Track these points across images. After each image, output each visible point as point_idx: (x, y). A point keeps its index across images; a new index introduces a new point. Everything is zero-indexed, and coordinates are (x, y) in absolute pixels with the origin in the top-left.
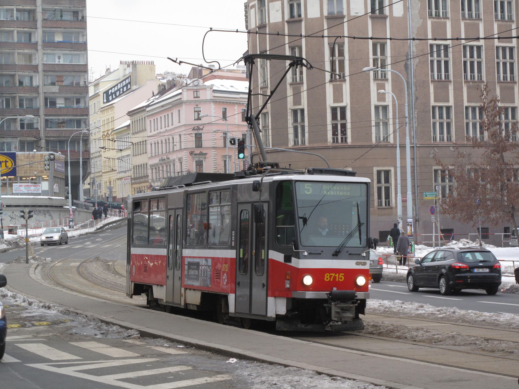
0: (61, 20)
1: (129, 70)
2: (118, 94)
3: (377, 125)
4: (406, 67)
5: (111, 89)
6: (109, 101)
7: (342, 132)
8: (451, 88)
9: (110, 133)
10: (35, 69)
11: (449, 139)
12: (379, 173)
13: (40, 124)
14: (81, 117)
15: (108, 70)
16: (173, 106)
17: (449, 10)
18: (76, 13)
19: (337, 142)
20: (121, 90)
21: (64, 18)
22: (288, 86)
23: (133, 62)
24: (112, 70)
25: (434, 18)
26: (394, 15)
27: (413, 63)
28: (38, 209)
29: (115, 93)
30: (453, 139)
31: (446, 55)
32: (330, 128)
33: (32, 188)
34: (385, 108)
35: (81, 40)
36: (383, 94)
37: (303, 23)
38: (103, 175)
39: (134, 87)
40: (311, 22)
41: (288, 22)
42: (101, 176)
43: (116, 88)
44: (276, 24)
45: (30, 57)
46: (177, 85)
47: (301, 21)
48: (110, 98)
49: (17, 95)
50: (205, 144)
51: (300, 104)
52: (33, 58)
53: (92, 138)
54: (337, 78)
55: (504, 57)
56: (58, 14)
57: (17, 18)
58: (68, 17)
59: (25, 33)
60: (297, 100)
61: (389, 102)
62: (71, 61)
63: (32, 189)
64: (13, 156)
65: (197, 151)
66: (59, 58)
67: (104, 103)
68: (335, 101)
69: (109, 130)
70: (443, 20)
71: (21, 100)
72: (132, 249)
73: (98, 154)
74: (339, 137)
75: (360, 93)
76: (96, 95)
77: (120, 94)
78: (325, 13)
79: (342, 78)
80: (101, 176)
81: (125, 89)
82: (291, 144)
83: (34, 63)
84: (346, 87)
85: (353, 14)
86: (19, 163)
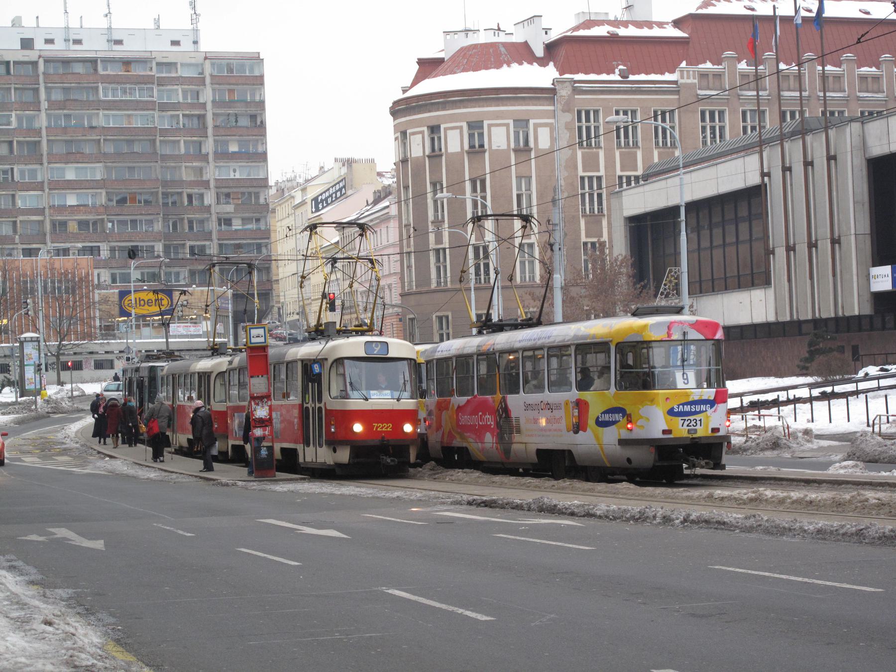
0: (236, 127)
1: (344, 170)
2: (329, 200)
5: (321, 194)
8: (605, 223)
10: (206, 184)
13: (213, 249)
16: (381, 222)
18: (253, 117)
19: (480, 282)
21: (239, 124)
22: (430, 224)
23: (348, 160)
24: (326, 169)
26: (540, 147)
28: (194, 353)
29: (326, 199)
33: (192, 329)
35: (260, 150)
37: (444, 158)
39: (349, 192)
41: (429, 157)
43: (327, 194)
44: (417, 158)
45: (201, 170)
47: (441, 155)
48: (320, 206)
49: (186, 216)
51: (442, 243)
52: (204, 172)
56: (233, 119)
57: (184, 125)
58: (244, 122)
59: (195, 142)
62: (249, 175)
63: (192, 330)
66: (235, 171)
71: (191, 222)
74: (482, 277)
76: (303, 203)
77: (332, 201)
81: (338, 194)
82: (434, 285)
83: (204, 178)
85: (494, 147)
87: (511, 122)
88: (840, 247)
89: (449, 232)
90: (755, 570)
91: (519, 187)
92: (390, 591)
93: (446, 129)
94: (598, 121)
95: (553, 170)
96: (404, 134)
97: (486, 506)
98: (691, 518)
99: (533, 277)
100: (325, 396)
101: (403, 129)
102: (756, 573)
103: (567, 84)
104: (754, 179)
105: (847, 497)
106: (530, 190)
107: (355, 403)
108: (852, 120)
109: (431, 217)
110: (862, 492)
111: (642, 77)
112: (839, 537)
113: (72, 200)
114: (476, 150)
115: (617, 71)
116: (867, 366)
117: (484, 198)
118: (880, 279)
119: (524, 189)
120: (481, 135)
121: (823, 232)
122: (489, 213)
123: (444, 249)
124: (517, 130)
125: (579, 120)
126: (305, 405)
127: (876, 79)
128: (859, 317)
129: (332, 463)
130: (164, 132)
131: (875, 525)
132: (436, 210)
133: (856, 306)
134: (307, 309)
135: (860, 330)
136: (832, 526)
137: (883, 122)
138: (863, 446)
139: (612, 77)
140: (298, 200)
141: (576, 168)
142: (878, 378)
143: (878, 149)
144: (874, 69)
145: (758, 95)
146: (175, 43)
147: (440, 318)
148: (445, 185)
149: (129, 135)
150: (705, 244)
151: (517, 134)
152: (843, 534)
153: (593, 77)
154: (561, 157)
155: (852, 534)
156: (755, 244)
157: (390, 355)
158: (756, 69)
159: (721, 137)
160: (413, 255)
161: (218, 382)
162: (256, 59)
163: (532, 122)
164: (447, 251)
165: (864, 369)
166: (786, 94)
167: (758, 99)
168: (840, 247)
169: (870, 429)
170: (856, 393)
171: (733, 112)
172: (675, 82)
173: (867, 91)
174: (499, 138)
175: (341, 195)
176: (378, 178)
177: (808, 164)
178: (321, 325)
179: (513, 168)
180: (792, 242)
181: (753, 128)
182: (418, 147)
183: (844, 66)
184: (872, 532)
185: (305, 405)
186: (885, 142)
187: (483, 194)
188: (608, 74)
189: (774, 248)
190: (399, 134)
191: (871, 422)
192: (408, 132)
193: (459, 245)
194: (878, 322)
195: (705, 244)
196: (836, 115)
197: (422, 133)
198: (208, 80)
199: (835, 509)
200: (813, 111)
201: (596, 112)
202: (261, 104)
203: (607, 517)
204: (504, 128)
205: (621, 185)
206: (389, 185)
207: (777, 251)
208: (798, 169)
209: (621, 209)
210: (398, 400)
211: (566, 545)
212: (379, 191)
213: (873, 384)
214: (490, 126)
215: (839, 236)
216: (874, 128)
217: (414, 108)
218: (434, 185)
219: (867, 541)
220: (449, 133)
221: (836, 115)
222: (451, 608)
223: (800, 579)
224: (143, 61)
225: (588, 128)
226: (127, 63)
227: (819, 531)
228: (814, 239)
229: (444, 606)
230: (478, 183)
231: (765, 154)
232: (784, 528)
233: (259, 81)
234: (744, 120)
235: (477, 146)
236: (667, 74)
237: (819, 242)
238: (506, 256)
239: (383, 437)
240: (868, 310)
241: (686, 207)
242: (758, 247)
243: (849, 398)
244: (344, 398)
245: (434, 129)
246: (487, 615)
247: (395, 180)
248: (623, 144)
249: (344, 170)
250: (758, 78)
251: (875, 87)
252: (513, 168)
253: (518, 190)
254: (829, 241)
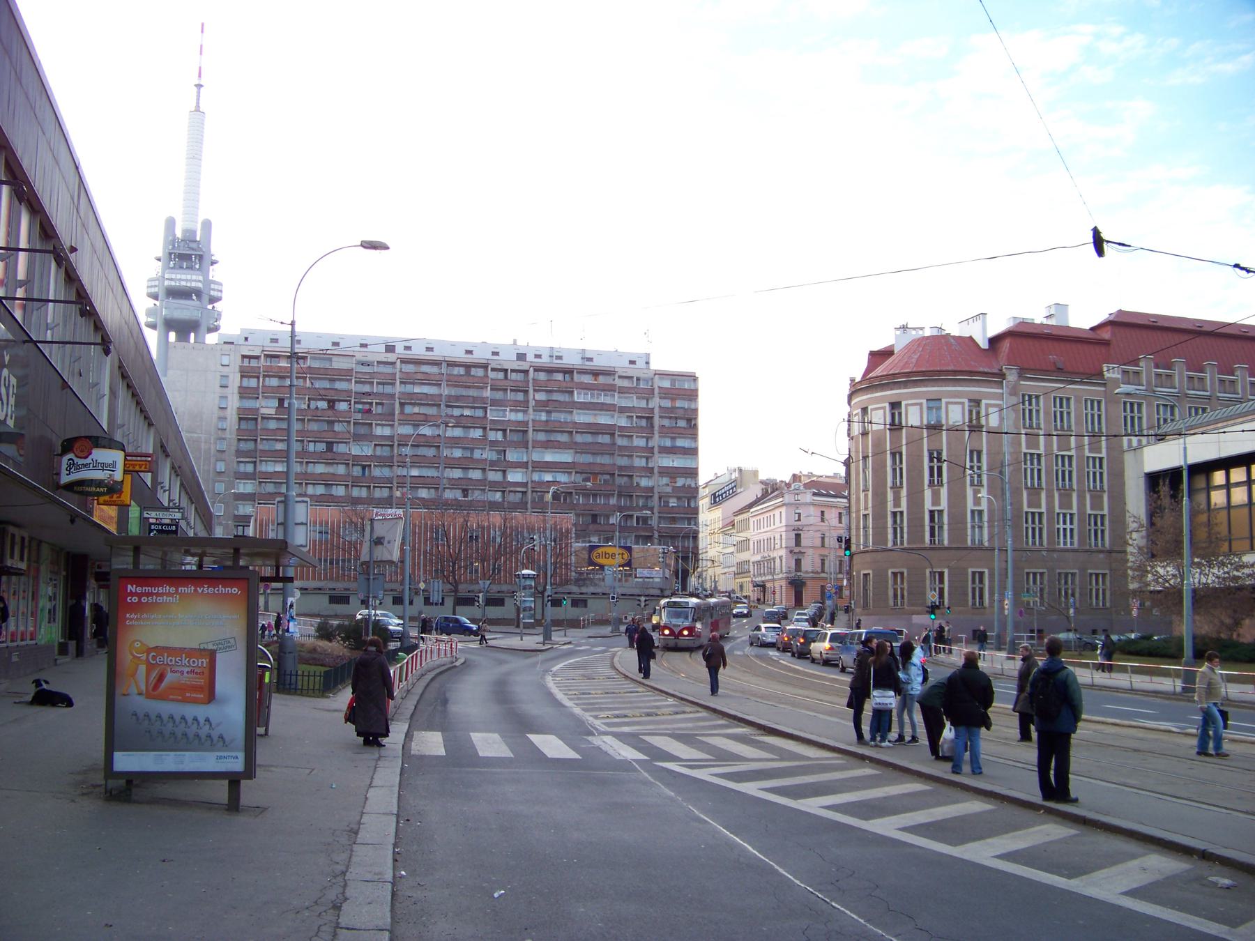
3: (973, 527)
4: (1001, 473)
8: (1075, 496)
11: (1041, 544)
12: (974, 573)
14: (692, 514)
17: (1042, 421)
18: (689, 420)
27: (1007, 470)
30: (1045, 543)
31: (1039, 463)
32: (927, 529)
34: (980, 512)
36: (980, 499)
50: (804, 542)
53: (700, 535)
54: (935, 483)
55: (1094, 467)
58: (682, 423)
60: (897, 502)
61: (984, 506)
64: (629, 549)
65: (797, 550)
68: (933, 504)
71: (638, 518)
72: (118, 756)
75: (957, 498)
78: (925, 422)
79: (940, 484)
82: (890, 545)
84: (944, 492)
85: (951, 423)
86: (635, 555)
87: (966, 401)
109: (889, 484)
113: (548, 477)
125: (1023, 403)
130: (621, 428)
132: (894, 477)
146: (632, 362)
147: (895, 574)
149: (595, 429)
151: (970, 412)
162: (693, 378)
163: (984, 402)
171: (1149, 405)
197: (884, 408)
198: (656, 391)
202: (696, 410)
214: (947, 403)
220: (911, 409)
224: (609, 373)
226: (596, 374)
233: (692, 395)
245: (895, 406)
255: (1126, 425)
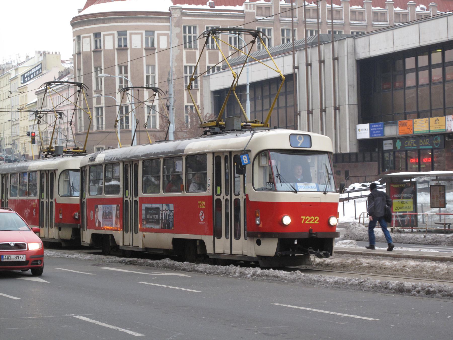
1: (41, 58)
2: (32, 76)
5: (27, 73)
6: (26, 82)
7: (126, 122)
8: (199, 94)
9: (24, 106)
15: (28, 57)
19: (123, 128)
20: (35, 73)
22: (93, 92)
23: (44, 53)
24: (30, 58)
25: (187, 49)
26: (161, 48)
29: (30, 76)
37: (102, 53)
38: (20, 138)
39: (44, 72)
40: (107, 52)
41: (94, 51)
42: (19, 139)
43: (31, 73)
44: (87, 52)
46: (71, 72)
47: (101, 51)
48: (26, 80)
51: (100, 104)
67: (21, 83)
69: (23, 105)
70: (193, 50)
73: (17, 122)
76: (16, 78)
77: (34, 77)
80: (19, 139)
82: (95, 129)
85: (133, 47)
87: (144, 32)
88: (339, 112)
89: (105, 97)
90: (300, 306)
91: (148, 71)
92: (77, 317)
93: (104, 35)
94: (196, 33)
95: (168, 62)
96: (79, 37)
97: (131, 264)
98: (257, 273)
99: (155, 125)
100: (56, 195)
101: (78, 35)
102: (301, 308)
103: (178, 10)
104: (289, 71)
105: (350, 262)
106: (154, 73)
107: (283, 195)
108: (348, 37)
110: (358, 259)
111: (223, 7)
112: (348, 287)
114: (122, 48)
115: (208, 3)
116: (354, 183)
117: (127, 77)
118: (363, 132)
119: (150, 72)
120: (125, 39)
121: (330, 103)
122: (129, 86)
123: (102, 108)
124: (147, 37)
125: (185, 32)
126: (41, 200)
127: (361, 13)
128: (350, 154)
129: (254, 255)
131: (370, 279)
132: (97, 84)
133: (348, 147)
134: (17, 142)
135: (350, 161)
136: (344, 280)
137: (366, 38)
138: (354, 231)
139: (205, 7)
140: (13, 76)
141: (182, 60)
142: (361, 190)
143: (363, 54)
144: (360, 7)
145: (292, 21)
148: (103, 68)
150: (259, 108)
151: (147, 39)
152: (351, 285)
153: (193, 6)
154: (174, 53)
155: (356, 285)
156: (289, 109)
157: (314, 148)
158: (292, 5)
159: (269, 45)
160: (82, 111)
161: (63, 178)
163: (156, 32)
164: (104, 109)
165: (352, 185)
166: (308, 20)
167: (293, 23)
168: (339, 112)
169: (358, 221)
170: (348, 199)
172: (242, 11)
173: (356, 20)
174: (136, 41)
175: (39, 74)
176: (62, 64)
177: (321, 62)
178: (52, 148)
179: (144, 58)
180: (311, 109)
181: (288, 40)
182: (87, 46)
183: (342, 5)
184: (368, 284)
185: (41, 200)
186: (367, 50)
187: (126, 75)
188: (203, 5)
189: (300, 112)
190: (75, 37)
191: (358, 216)
192: (81, 36)
193: (111, 105)
194: (360, 157)
195: (259, 108)
196: (337, 33)
197: (90, 37)
199: (342, 269)
200: (325, 31)
201: (195, 28)
203: (205, 272)
204: (140, 36)
205: (208, 71)
206: (69, 68)
207: (302, 113)
208: (316, 65)
209: (209, 86)
210: (325, 193)
211: (182, 289)
212: (62, 72)
213: (358, 194)
214: (131, 34)
215: (339, 106)
216: (361, 41)
217: (85, 21)
218: (96, 68)
219: (365, 289)
220: (106, 37)
221: (337, 33)
222: (116, 328)
223: (328, 312)
225: (190, 37)
227: (336, 283)
228: (324, 107)
229: (112, 327)
230: (123, 68)
231: (296, 55)
232: (315, 280)
234: (283, 35)
235: (123, 46)
236: (237, 6)
237: (327, 109)
238: (139, 112)
239: (310, 230)
240: (355, 150)
241: (250, 86)
242: (290, 111)
243: (345, 202)
244: (271, 190)
245: (97, 35)
246: (139, 333)
247: (73, 65)
248: (210, 47)
249: (41, 58)
250: (292, 9)
251: (361, 18)
252: (144, 58)
253: (147, 73)
254: (333, 108)
255: (231, 43)
